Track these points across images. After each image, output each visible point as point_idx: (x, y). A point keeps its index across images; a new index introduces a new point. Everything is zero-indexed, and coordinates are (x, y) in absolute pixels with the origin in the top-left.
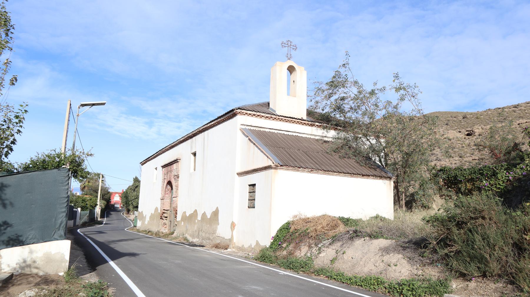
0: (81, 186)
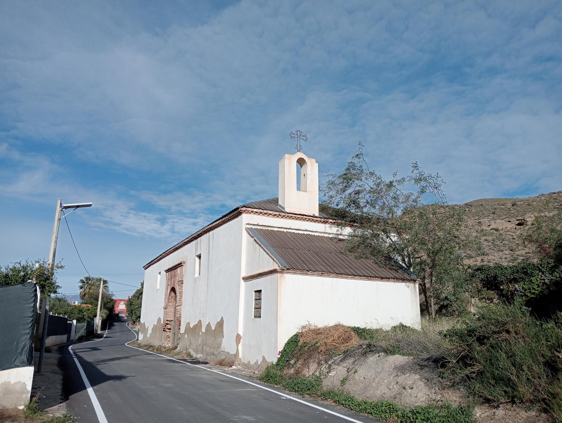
0: (80, 294)
